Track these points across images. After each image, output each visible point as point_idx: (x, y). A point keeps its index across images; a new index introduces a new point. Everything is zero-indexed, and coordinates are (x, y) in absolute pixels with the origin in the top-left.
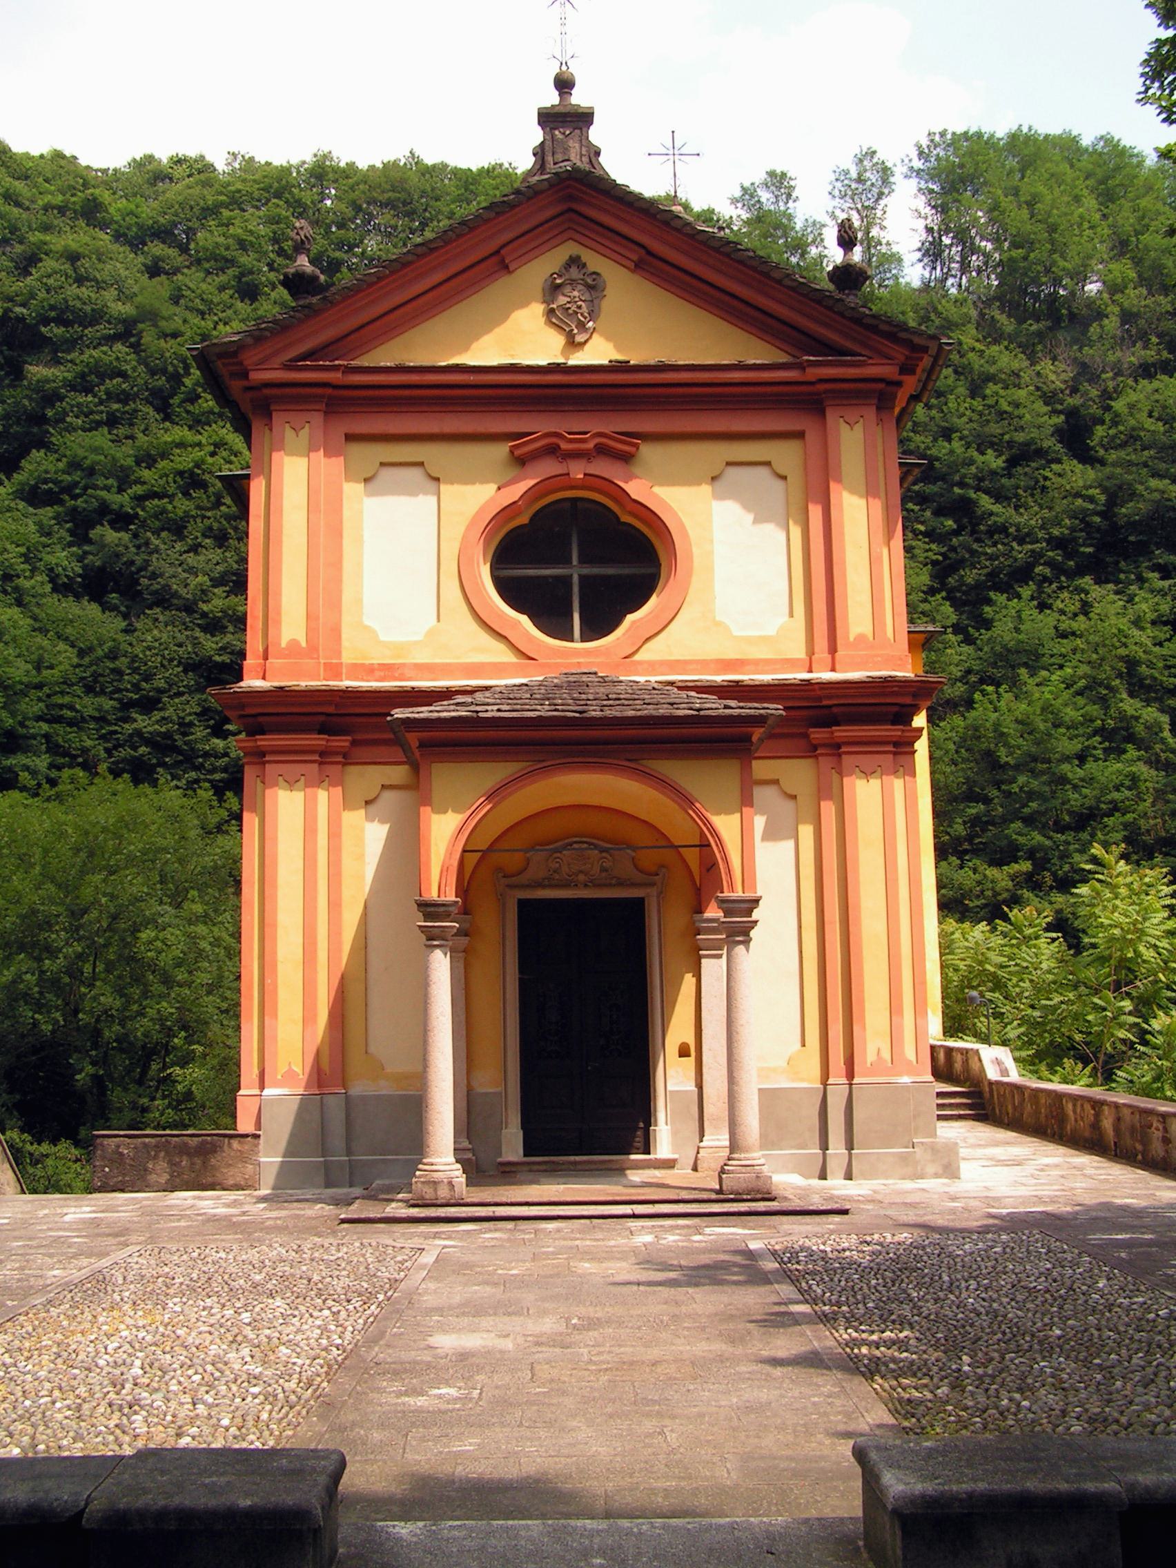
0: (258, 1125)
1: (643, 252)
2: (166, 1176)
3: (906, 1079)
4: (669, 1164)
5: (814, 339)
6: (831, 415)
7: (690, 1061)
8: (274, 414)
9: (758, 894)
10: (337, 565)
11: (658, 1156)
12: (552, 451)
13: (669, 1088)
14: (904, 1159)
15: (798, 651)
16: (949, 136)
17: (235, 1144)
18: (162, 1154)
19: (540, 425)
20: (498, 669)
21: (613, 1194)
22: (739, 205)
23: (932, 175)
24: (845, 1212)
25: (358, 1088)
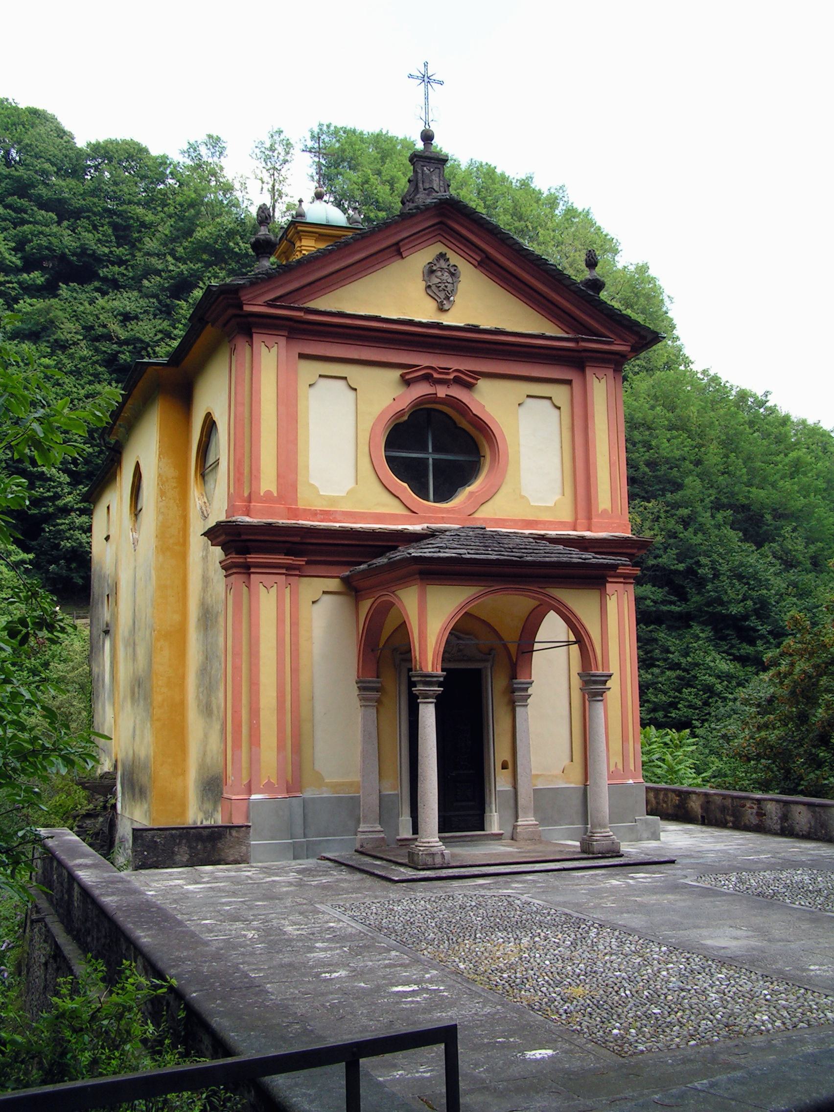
0: (248, 818)
1: (484, 256)
2: (187, 856)
3: (631, 781)
4: (498, 837)
5: (581, 324)
6: (589, 372)
7: (508, 773)
8: (254, 335)
9: (611, 672)
10: (295, 442)
11: (493, 832)
12: (427, 378)
13: (497, 789)
14: (631, 829)
15: (566, 515)
16: (332, 128)
17: (234, 833)
18: (184, 841)
19: (423, 360)
20: (394, 518)
21: (532, 857)
22: (186, 155)
23: (317, 152)
24: (673, 862)
25: (309, 793)
